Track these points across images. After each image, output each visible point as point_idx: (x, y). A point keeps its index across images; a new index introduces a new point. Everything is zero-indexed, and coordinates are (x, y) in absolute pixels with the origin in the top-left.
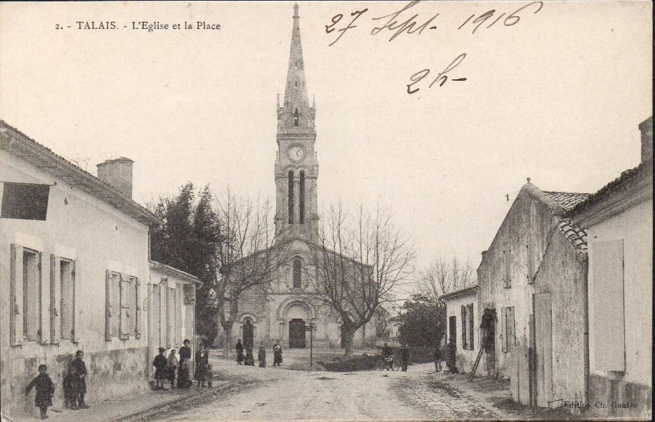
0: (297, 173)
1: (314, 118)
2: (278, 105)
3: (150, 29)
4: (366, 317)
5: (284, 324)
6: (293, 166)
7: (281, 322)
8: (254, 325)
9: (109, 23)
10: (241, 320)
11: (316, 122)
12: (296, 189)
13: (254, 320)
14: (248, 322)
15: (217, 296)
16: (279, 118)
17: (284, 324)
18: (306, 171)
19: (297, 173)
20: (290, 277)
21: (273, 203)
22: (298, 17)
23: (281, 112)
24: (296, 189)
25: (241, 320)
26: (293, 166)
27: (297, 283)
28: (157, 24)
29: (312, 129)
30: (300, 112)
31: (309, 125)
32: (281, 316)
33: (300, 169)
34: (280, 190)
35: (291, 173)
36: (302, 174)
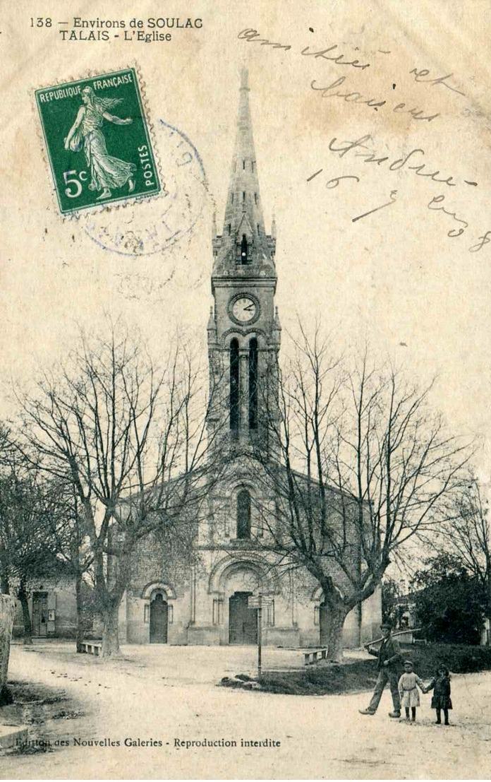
0: (244, 342)
1: (273, 253)
2: (215, 230)
3: (147, 40)
4: (371, 577)
5: (220, 601)
6: (239, 331)
7: (216, 597)
8: (169, 602)
9: (101, 33)
10: (147, 594)
11: (277, 258)
12: (244, 366)
13: (170, 593)
14: (159, 596)
15: (96, 556)
16: (216, 253)
17: (220, 601)
18: (261, 340)
19: (244, 342)
20: (233, 523)
21: (203, 383)
22: (249, 90)
23: (219, 243)
24: (244, 366)
25: (147, 594)
26: (239, 331)
27: (243, 532)
28: (155, 33)
29: (270, 268)
30: (249, 241)
31: (266, 262)
32: (215, 588)
33: (253, 335)
34: (215, 371)
35: (235, 343)
36: (254, 343)
